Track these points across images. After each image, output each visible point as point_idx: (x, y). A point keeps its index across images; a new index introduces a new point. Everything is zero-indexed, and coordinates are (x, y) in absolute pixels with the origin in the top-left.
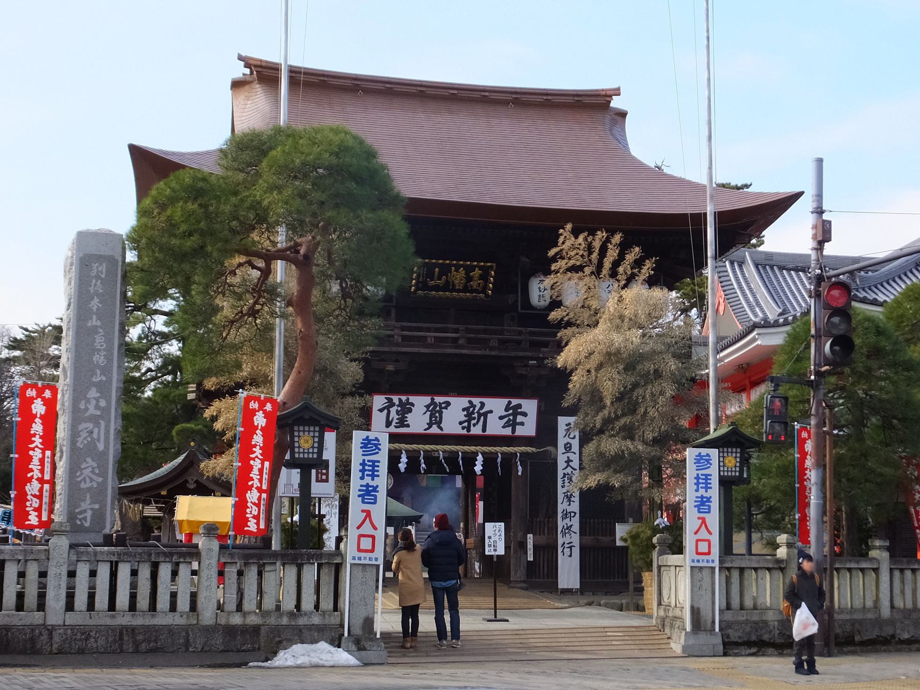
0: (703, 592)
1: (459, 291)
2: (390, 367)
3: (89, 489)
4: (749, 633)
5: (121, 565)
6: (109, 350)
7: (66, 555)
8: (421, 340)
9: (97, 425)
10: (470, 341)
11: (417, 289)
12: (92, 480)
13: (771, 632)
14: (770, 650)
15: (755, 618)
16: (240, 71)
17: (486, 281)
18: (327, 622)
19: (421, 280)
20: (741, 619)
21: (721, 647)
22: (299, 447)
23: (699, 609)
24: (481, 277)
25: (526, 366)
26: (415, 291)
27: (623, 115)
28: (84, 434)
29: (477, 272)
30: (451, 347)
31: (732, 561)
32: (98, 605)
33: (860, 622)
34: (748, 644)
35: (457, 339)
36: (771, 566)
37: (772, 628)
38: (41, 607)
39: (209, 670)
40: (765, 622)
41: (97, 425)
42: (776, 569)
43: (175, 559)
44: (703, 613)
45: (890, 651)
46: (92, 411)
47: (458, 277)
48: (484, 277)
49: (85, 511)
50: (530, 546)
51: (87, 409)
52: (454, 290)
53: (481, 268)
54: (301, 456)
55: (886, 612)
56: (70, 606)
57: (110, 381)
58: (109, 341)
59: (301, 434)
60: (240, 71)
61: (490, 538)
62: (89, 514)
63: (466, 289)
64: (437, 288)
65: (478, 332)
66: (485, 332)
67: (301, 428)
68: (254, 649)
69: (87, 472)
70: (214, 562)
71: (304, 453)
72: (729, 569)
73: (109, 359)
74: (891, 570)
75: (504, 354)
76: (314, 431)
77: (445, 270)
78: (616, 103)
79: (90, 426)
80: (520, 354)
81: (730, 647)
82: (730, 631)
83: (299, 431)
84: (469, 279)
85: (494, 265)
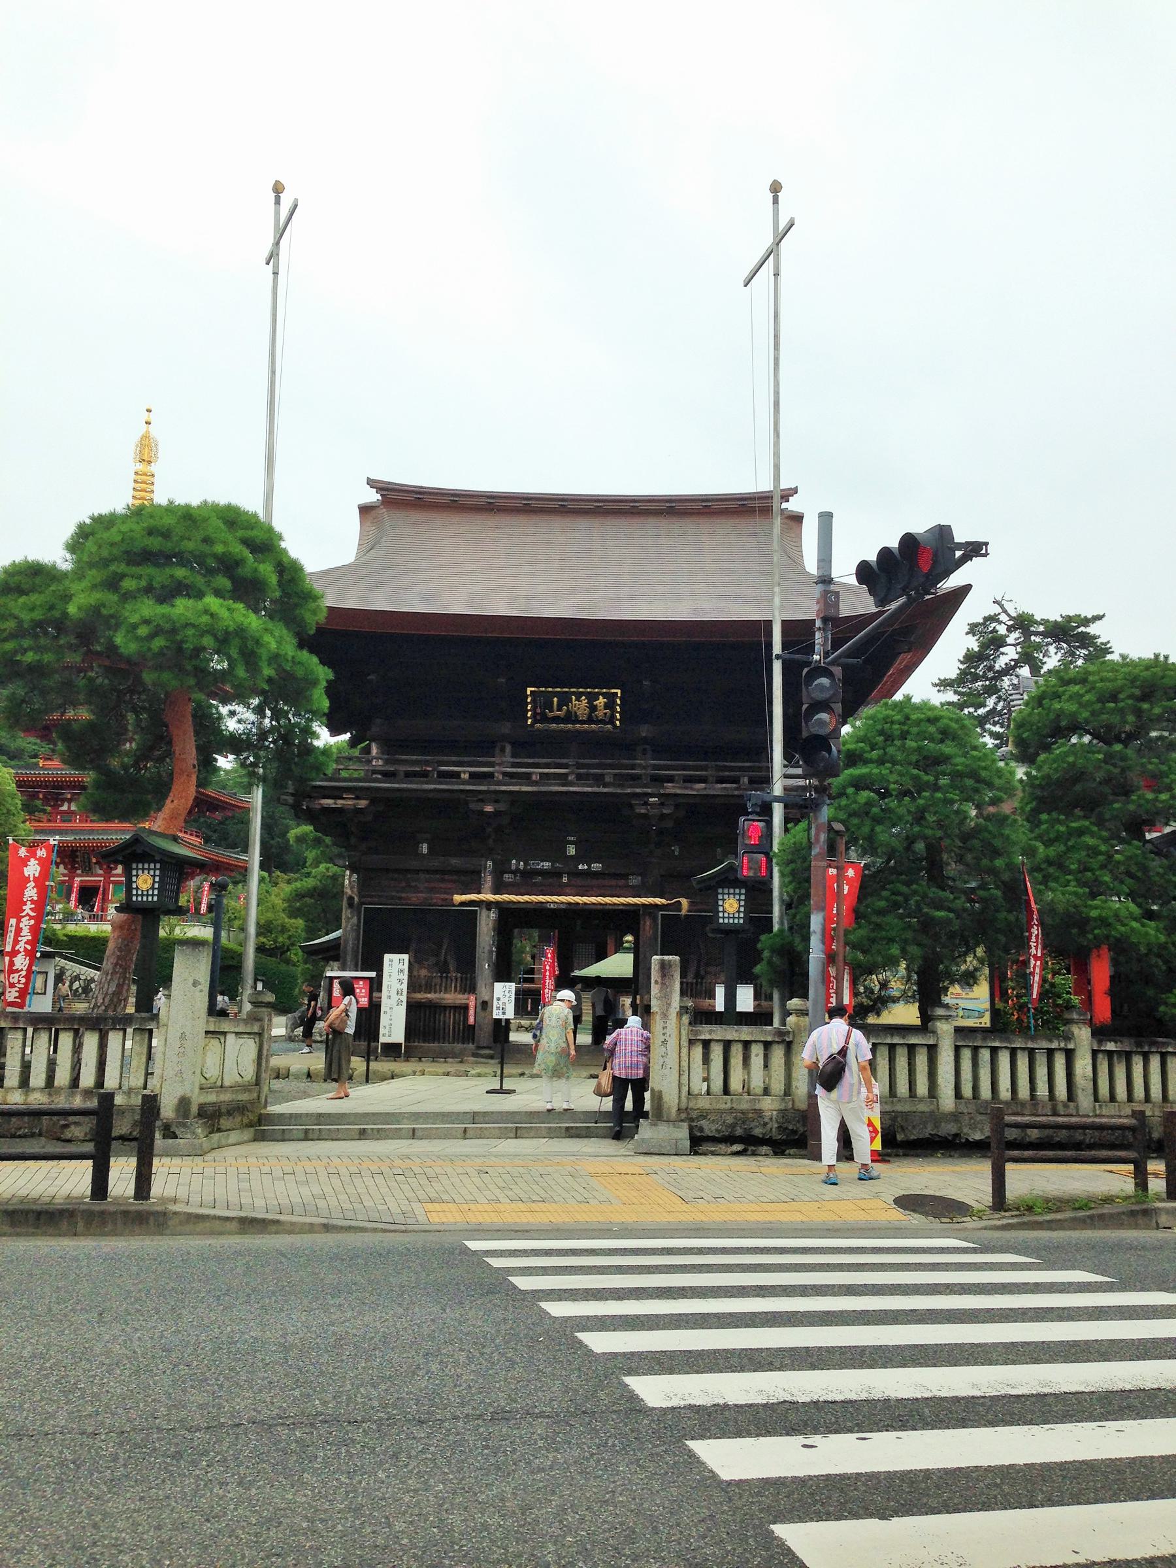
0: (667, 1071)
1: (583, 722)
2: (489, 809)
4: (733, 1126)
8: (599, 780)
10: (579, 777)
11: (535, 721)
13: (765, 1124)
14: (765, 1149)
15: (744, 1106)
16: (373, 497)
17: (613, 711)
19: (538, 711)
20: (724, 1106)
21: (688, 1143)
22: (724, 912)
23: (660, 1092)
24: (606, 706)
25: (646, 804)
26: (532, 725)
29: (601, 701)
30: (559, 785)
33: (906, 1115)
34: (729, 1139)
35: (566, 775)
36: (769, 1039)
37: (766, 1120)
40: (759, 1113)
42: (778, 1042)
47: (580, 706)
48: (610, 705)
53: (604, 695)
54: (140, 899)
59: (140, 872)
60: (373, 497)
61: (498, 999)
63: (590, 720)
64: (556, 720)
65: (548, 766)
66: (732, 769)
67: (726, 891)
68: (33, 1135)
71: (142, 895)
72: (706, 1044)
74: (957, 1049)
75: (619, 791)
76: (740, 894)
77: (565, 700)
80: (638, 790)
81: (698, 1143)
82: (704, 1123)
83: (137, 869)
84: (593, 708)
85: (619, 691)
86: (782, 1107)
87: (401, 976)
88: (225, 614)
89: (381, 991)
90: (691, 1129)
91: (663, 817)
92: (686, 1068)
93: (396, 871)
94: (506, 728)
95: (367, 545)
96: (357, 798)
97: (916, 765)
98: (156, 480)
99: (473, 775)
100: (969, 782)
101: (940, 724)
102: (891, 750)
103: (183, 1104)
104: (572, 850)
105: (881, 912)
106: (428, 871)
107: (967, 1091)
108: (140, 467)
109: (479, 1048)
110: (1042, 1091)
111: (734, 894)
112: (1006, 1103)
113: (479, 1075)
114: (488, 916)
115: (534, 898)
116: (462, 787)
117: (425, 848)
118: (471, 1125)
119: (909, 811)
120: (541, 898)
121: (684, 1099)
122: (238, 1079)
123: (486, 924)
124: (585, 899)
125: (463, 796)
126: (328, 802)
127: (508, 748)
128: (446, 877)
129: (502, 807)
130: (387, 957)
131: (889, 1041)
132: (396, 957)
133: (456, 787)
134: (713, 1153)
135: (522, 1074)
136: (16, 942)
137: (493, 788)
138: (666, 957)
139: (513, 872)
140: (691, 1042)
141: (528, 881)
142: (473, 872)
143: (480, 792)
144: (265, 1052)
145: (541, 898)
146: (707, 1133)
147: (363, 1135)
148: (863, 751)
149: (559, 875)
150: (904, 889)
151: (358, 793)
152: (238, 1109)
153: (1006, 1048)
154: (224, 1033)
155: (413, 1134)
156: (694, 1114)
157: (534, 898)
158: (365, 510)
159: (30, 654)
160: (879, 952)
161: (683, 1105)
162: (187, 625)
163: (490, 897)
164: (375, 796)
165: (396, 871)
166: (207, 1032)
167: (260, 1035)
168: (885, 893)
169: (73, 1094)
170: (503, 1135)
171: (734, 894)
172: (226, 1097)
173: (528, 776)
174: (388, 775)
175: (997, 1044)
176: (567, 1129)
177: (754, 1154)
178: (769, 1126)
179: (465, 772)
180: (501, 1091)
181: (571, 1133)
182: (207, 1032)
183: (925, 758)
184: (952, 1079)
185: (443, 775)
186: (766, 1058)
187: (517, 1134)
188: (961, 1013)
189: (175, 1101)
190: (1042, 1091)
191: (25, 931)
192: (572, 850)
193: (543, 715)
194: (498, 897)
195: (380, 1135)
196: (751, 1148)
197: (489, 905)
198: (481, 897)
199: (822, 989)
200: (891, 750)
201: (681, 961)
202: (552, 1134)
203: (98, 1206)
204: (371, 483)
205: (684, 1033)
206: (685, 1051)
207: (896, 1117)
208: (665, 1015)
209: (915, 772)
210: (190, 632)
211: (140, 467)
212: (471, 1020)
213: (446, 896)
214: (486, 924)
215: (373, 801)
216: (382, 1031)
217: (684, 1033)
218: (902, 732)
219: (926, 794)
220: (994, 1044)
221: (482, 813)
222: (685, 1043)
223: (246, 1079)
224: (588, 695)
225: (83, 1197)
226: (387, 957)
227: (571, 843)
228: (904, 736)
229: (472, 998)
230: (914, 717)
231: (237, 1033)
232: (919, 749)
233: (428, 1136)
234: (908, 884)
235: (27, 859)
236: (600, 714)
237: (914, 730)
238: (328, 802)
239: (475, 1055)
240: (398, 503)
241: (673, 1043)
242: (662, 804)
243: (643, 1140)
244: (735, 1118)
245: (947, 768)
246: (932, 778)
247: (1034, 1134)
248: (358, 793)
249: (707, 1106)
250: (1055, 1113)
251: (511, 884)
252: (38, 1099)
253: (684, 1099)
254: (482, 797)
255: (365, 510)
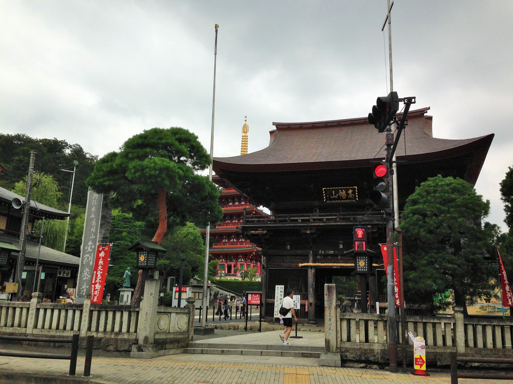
0: (331, 331)
1: (344, 199)
2: (308, 232)
3: (86, 280)
4: (360, 356)
5: (76, 311)
6: (97, 226)
7: (35, 306)
9: (91, 255)
12: (87, 277)
13: (375, 356)
14: (375, 366)
16: (274, 128)
17: (355, 195)
18: (130, 338)
21: (340, 362)
23: (329, 340)
27: (430, 118)
28: (86, 259)
29: (350, 191)
31: (350, 316)
32: (67, 328)
33: (441, 354)
34: (359, 361)
35: (336, 219)
36: (376, 319)
37: (375, 354)
38: (26, 327)
39: (252, 357)
40: (372, 351)
41: (91, 255)
42: (380, 321)
43: (74, 308)
44: (331, 342)
45: (437, 372)
46: (89, 250)
47: (343, 193)
48: (354, 192)
49: (84, 289)
50: (378, 307)
51: (88, 249)
52: (342, 199)
53: (351, 189)
55: (461, 347)
56: (35, 326)
57: (96, 238)
58: (97, 223)
60: (274, 128)
62: (85, 290)
64: (335, 199)
67: (360, 258)
68: (98, 349)
69: (86, 274)
70: (88, 310)
73: (97, 230)
74: (466, 326)
77: (337, 192)
78: (428, 114)
79: (88, 255)
81: (345, 363)
82: (348, 354)
86: (383, 348)
87: (281, 293)
88: (159, 162)
89: (274, 298)
90: (341, 356)
91: (373, 233)
92: (340, 331)
93: (279, 255)
94: (317, 203)
95: (272, 143)
96: (263, 230)
97: (440, 203)
98: (248, 138)
99: (302, 220)
100: (463, 209)
101: (452, 186)
102: (429, 198)
103: (146, 339)
104: (341, 246)
105: (424, 265)
106: (290, 255)
107: (471, 343)
108: (244, 134)
109: (309, 320)
110: (499, 344)
111: (363, 259)
112: (491, 350)
113: (304, 331)
114: (311, 271)
115: (328, 264)
116: (298, 225)
117: (289, 247)
118: (282, 351)
119: (436, 223)
120: (330, 264)
121: (339, 343)
122: (178, 329)
123: (311, 274)
124: (347, 265)
125: (299, 228)
126: (253, 232)
127: (318, 210)
128: (297, 257)
129: (313, 231)
130: (277, 286)
131: (432, 321)
132: (280, 286)
133: (296, 225)
134: (351, 367)
135: (320, 331)
136: (96, 279)
137: (309, 224)
138: (330, 285)
139: (321, 255)
140: (341, 320)
141: (326, 258)
142: (305, 255)
143: (306, 226)
144: (191, 320)
145: (330, 264)
146: (349, 358)
147: (223, 352)
148: (418, 199)
149: (337, 256)
150: (436, 256)
151: (263, 228)
152: (178, 341)
153: (490, 325)
154: (170, 313)
155: (242, 353)
156: (343, 350)
157: (328, 264)
158: (271, 133)
159: (107, 182)
160: (423, 283)
161: (339, 346)
162: (147, 167)
163: (312, 264)
164: (269, 229)
165: (279, 255)
166: (158, 312)
167: (189, 313)
168: (426, 257)
169: (111, 334)
170: (277, 355)
171: (363, 259)
172: (172, 336)
173: (322, 220)
174: (275, 221)
175: (485, 323)
176: (302, 353)
177: (370, 368)
178: (377, 357)
179: (300, 219)
180: (296, 337)
181: (304, 355)
182: (158, 312)
183: (444, 200)
184: (463, 339)
185: (292, 221)
186: (376, 328)
187: (282, 354)
188: (497, 310)
189: (143, 338)
190: (499, 344)
191: (99, 276)
192: (341, 246)
193: (330, 198)
194: (314, 264)
195: (229, 353)
196: (369, 366)
197: (311, 267)
198: (309, 264)
199: (392, 297)
200: (429, 198)
201: (336, 286)
202: (296, 355)
203: (72, 378)
204: (274, 124)
205: (338, 315)
206: (339, 323)
207: (436, 355)
208: (330, 308)
209: (438, 206)
210: (147, 170)
211: (244, 134)
212: (307, 310)
213: (296, 264)
214: (311, 274)
215: (268, 231)
216: (275, 313)
217: (338, 315)
218: (434, 190)
219: (443, 215)
220: (493, 324)
221: (306, 234)
222: (339, 320)
223: (183, 330)
224: (345, 189)
225: (81, 374)
226: (277, 286)
227: (341, 244)
228: (435, 192)
229: (307, 301)
230: (440, 184)
231: (177, 313)
232: (441, 197)
233: (247, 354)
234: (437, 253)
235: (101, 251)
236: (351, 196)
237: (440, 189)
238: (253, 232)
239: (308, 323)
240: (283, 130)
241: (333, 319)
242: (372, 228)
243: (321, 360)
244: (361, 352)
245: (453, 204)
246: (446, 208)
247: (504, 365)
248: (263, 228)
249: (349, 347)
250: (505, 356)
251: (321, 259)
252: (100, 335)
253: (339, 343)
254: (305, 228)
255: (271, 133)
